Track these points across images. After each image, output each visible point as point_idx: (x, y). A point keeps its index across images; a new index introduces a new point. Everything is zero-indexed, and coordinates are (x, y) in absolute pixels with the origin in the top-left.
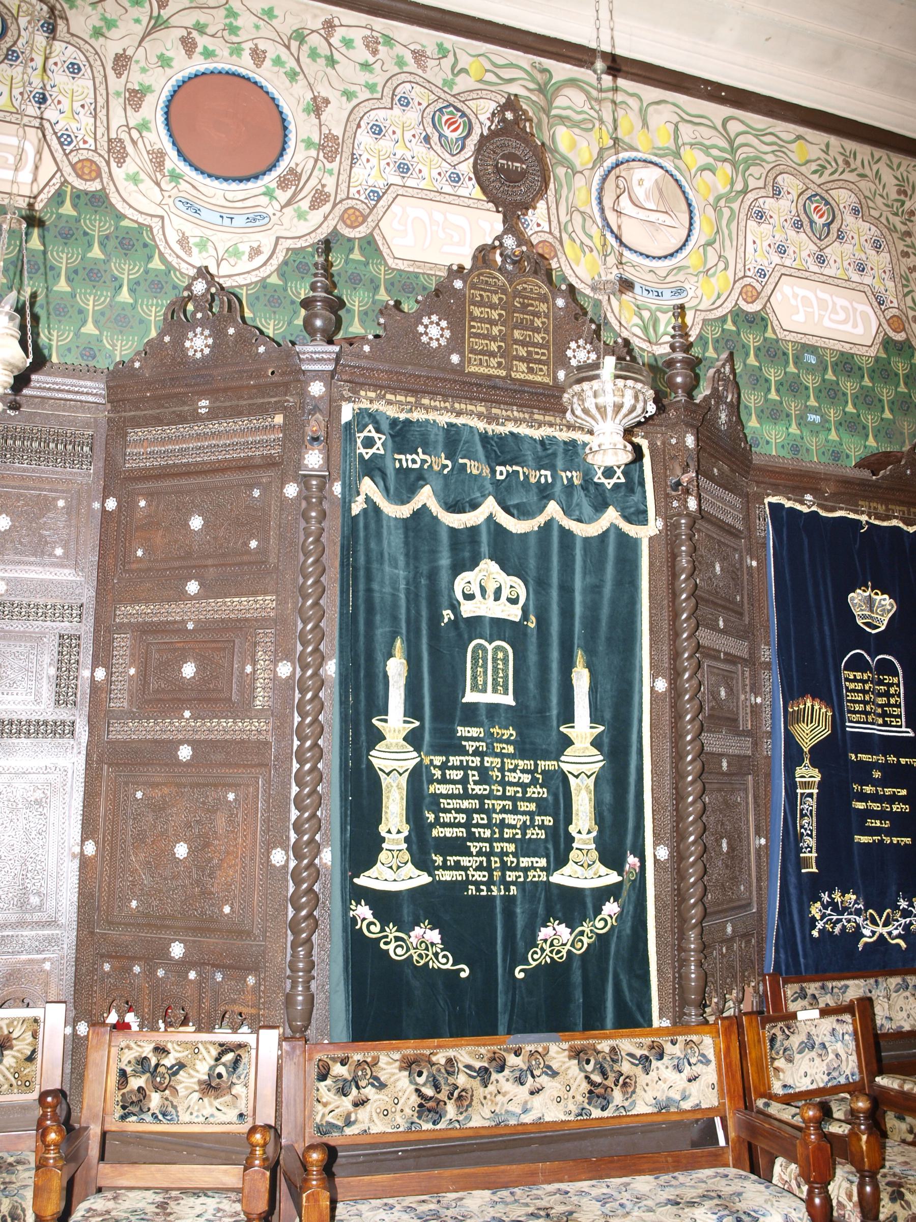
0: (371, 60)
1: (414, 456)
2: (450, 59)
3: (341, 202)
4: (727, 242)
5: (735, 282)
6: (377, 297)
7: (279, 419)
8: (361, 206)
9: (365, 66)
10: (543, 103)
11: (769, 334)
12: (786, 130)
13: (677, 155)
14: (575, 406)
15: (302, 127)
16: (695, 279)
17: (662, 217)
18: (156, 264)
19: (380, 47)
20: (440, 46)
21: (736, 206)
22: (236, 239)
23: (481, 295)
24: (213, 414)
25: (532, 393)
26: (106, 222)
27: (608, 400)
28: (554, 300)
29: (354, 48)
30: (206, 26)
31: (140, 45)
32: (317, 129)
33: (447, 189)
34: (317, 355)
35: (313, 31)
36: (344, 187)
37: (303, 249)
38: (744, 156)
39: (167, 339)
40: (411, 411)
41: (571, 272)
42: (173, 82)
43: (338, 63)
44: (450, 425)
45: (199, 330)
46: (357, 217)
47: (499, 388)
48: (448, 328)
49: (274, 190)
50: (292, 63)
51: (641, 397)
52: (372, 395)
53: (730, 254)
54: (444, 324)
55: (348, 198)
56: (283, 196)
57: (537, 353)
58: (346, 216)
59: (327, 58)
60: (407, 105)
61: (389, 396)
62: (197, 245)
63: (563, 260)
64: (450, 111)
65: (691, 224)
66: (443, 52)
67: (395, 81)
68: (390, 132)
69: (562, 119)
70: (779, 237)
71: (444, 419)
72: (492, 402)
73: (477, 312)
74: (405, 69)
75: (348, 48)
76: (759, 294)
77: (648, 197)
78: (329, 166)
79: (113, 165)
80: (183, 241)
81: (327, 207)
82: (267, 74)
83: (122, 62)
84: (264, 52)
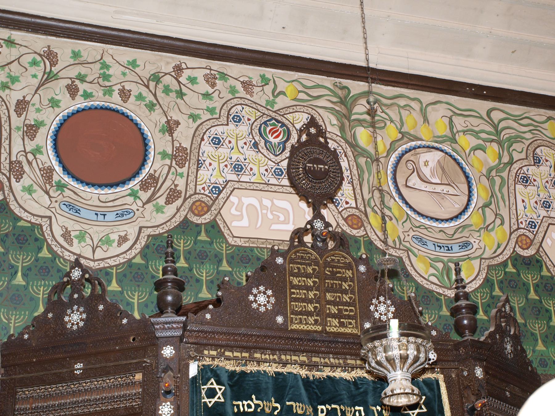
0: (211, 90)
1: (249, 402)
2: (271, 85)
3: (190, 197)
4: (501, 203)
5: (511, 234)
6: (220, 269)
7: (139, 377)
8: (205, 199)
9: (207, 96)
10: (344, 111)
11: (545, 273)
12: (538, 114)
13: (453, 140)
14: (370, 359)
15: (158, 143)
16: (478, 234)
17: (446, 189)
18: (45, 253)
19: (217, 81)
20: (263, 77)
21: (505, 174)
22: (108, 230)
23: (298, 268)
24: (87, 374)
25: (344, 343)
26: (6, 223)
27: (395, 353)
28: (357, 266)
29: (197, 83)
30: (86, 76)
31: (36, 92)
32: (170, 144)
33: (273, 181)
34: (169, 324)
35: (166, 74)
36: (192, 185)
37: (160, 234)
38: (507, 136)
39: (50, 315)
40: (245, 365)
41: (375, 237)
42: (60, 117)
43: (185, 95)
44: (278, 374)
45: (75, 307)
46: (203, 208)
47: (317, 341)
48: (273, 296)
49: (137, 191)
50: (152, 98)
51: (422, 349)
52: (214, 353)
53: (504, 212)
54: (270, 292)
55: (195, 193)
56: (145, 196)
57: (346, 310)
58: (194, 207)
59: (177, 92)
60: (239, 121)
61: (227, 353)
62: (77, 237)
63: (368, 228)
64: (273, 122)
65: (470, 192)
66: (265, 81)
67: (229, 105)
68: (227, 142)
71: (271, 369)
72: (312, 352)
73: (295, 281)
74: (237, 95)
75: (193, 84)
76: (532, 241)
77: (433, 174)
78: (180, 170)
79: (13, 180)
80: (66, 235)
81: (179, 202)
82: (132, 107)
83: (22, 106)
84: (130, 91)
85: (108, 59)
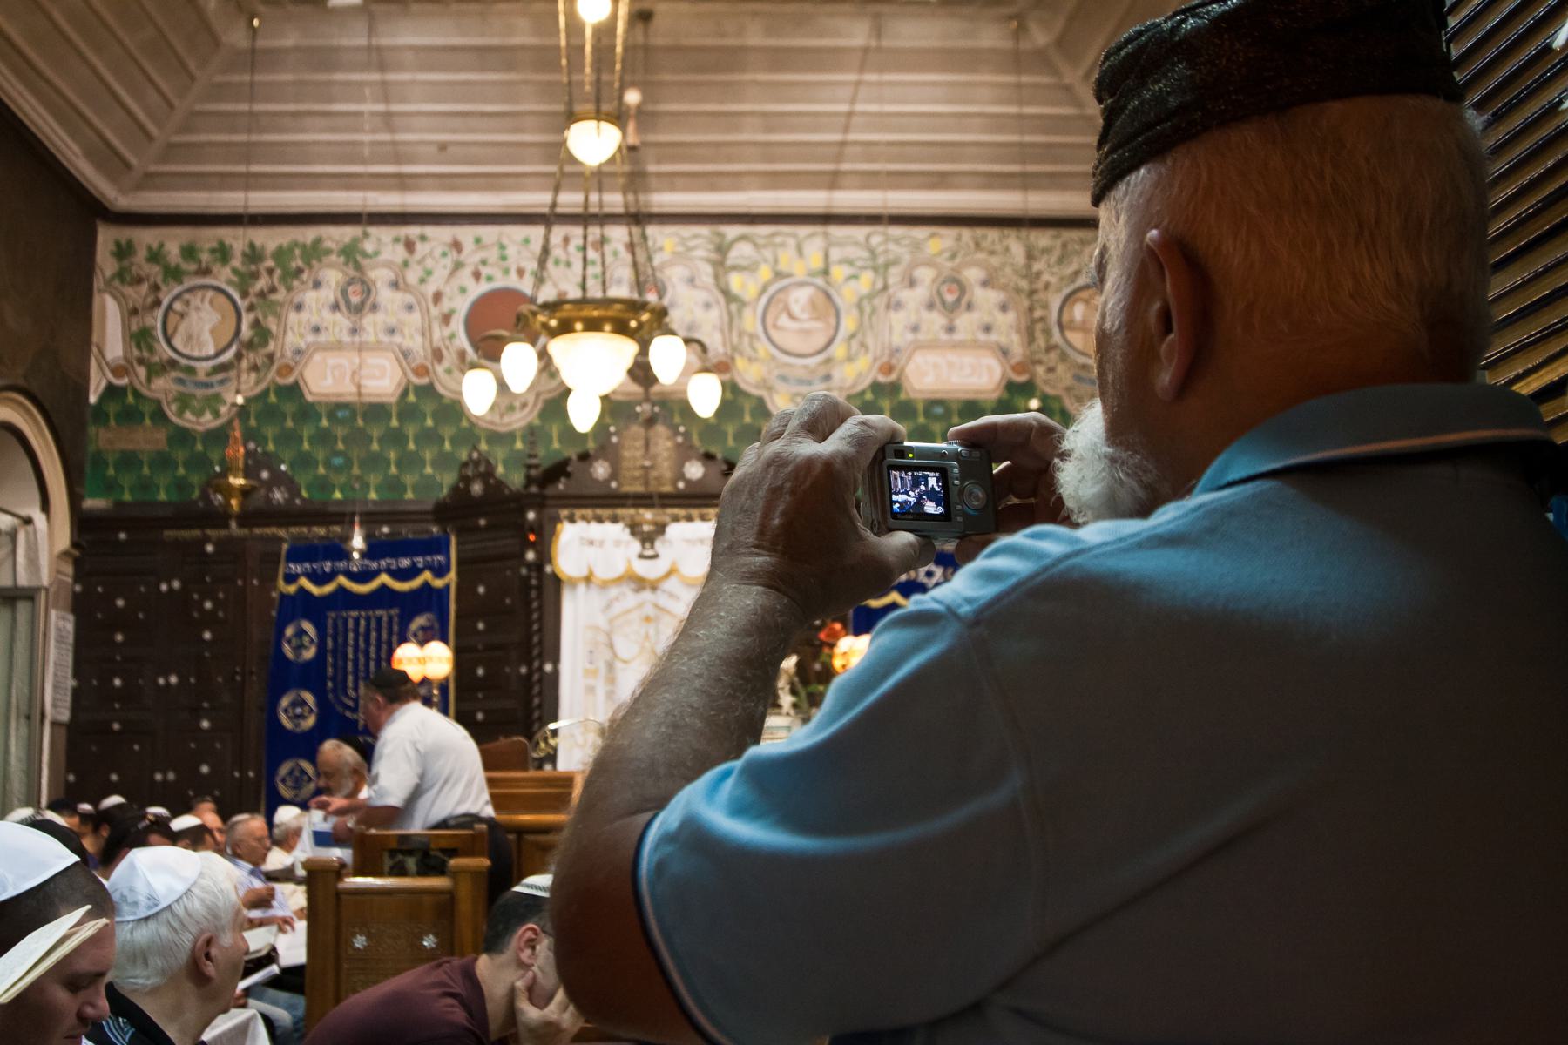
12: (920, 232)
18: (465, 424)
69: (735, 268)
70: (913, 319)
77: (803, 310)
83: (437, 297)
85: (505, 241)
